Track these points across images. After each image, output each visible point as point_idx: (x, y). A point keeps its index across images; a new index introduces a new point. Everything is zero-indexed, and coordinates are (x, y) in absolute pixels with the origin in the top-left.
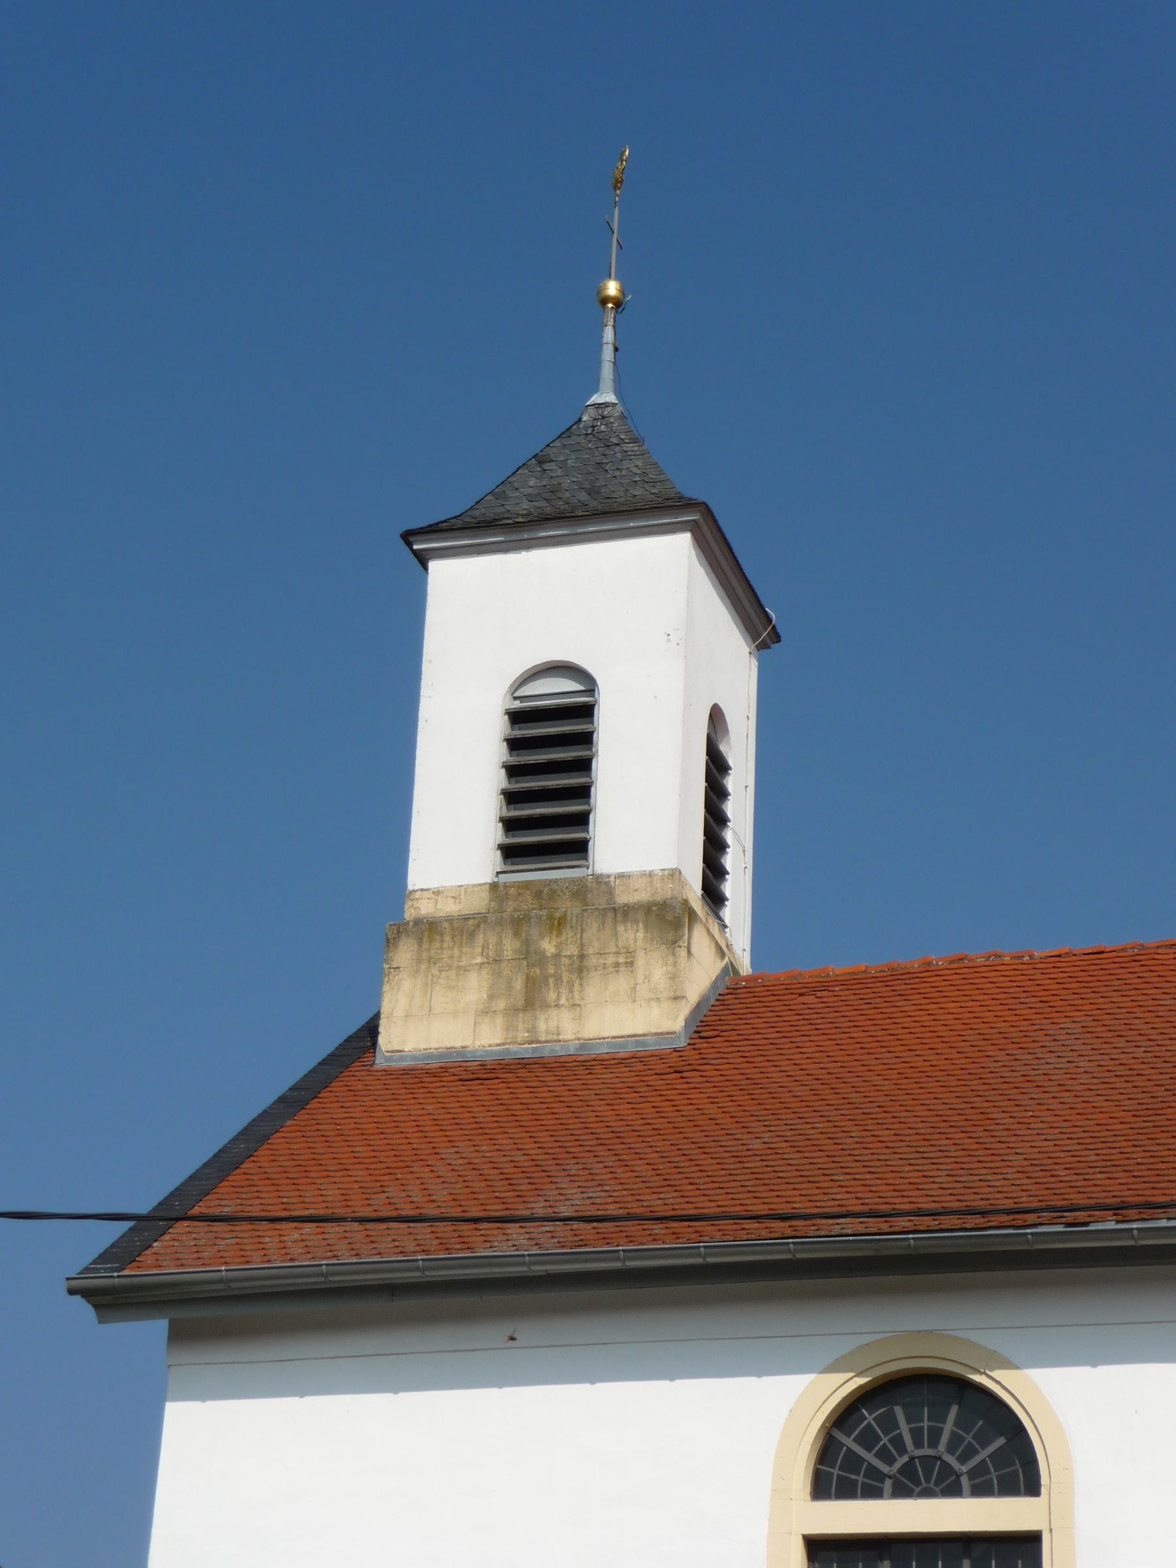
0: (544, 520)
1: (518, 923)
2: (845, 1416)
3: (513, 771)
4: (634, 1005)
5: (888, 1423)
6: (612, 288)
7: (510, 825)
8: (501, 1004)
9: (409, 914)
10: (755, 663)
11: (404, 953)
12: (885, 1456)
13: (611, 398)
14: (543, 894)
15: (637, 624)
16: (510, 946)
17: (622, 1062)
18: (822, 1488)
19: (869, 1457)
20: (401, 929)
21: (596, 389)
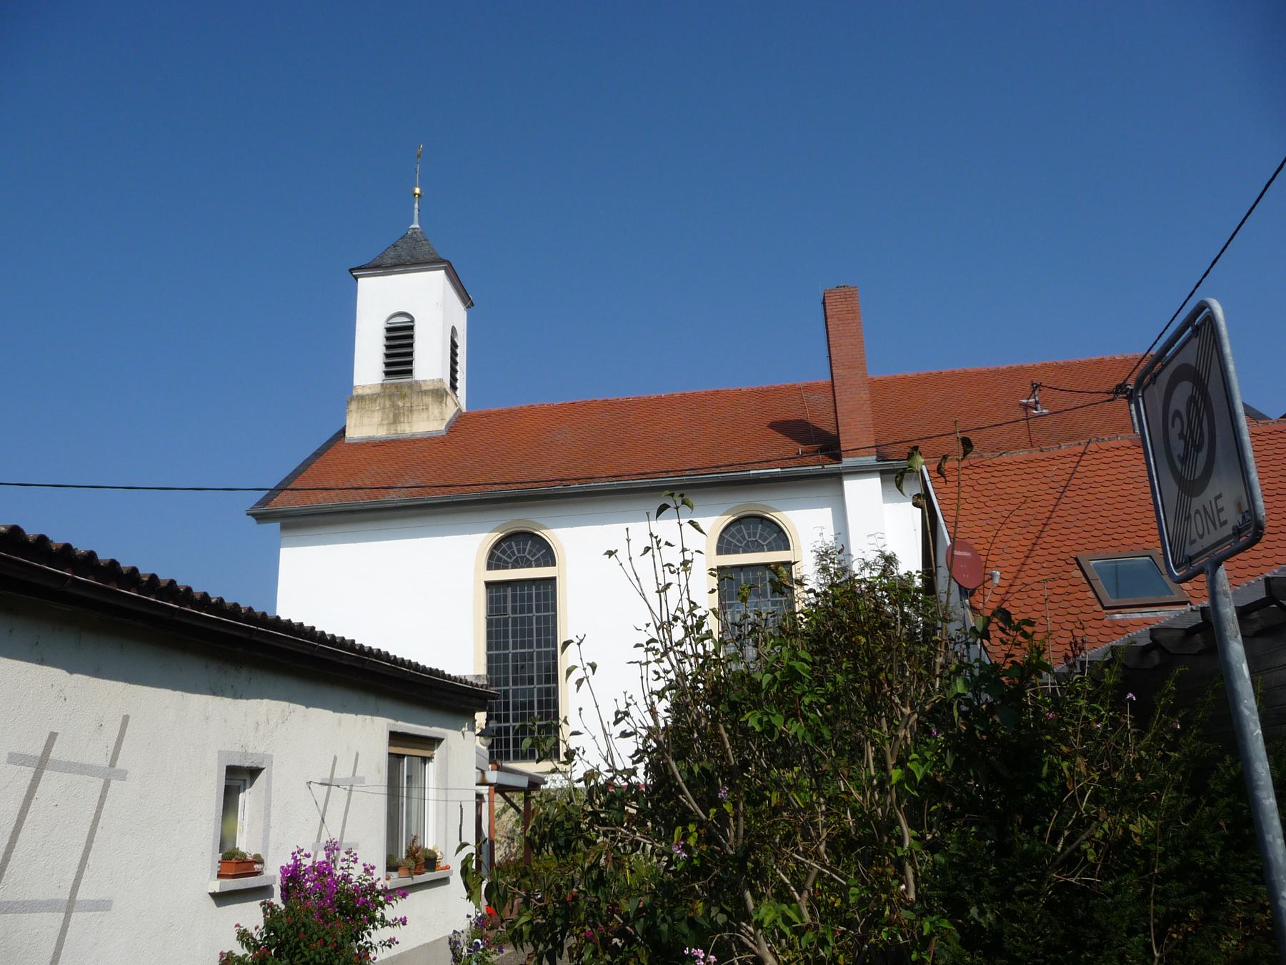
1: (391, 396)
2: (497, 546)
4: (428, 422)
5: (510, 547)
6: (417, 190)
7: (387, 365)
9: (355, 393)
11: (353, 406)
15: (427, 299)
18: (489, 567)
20: (352, 398)
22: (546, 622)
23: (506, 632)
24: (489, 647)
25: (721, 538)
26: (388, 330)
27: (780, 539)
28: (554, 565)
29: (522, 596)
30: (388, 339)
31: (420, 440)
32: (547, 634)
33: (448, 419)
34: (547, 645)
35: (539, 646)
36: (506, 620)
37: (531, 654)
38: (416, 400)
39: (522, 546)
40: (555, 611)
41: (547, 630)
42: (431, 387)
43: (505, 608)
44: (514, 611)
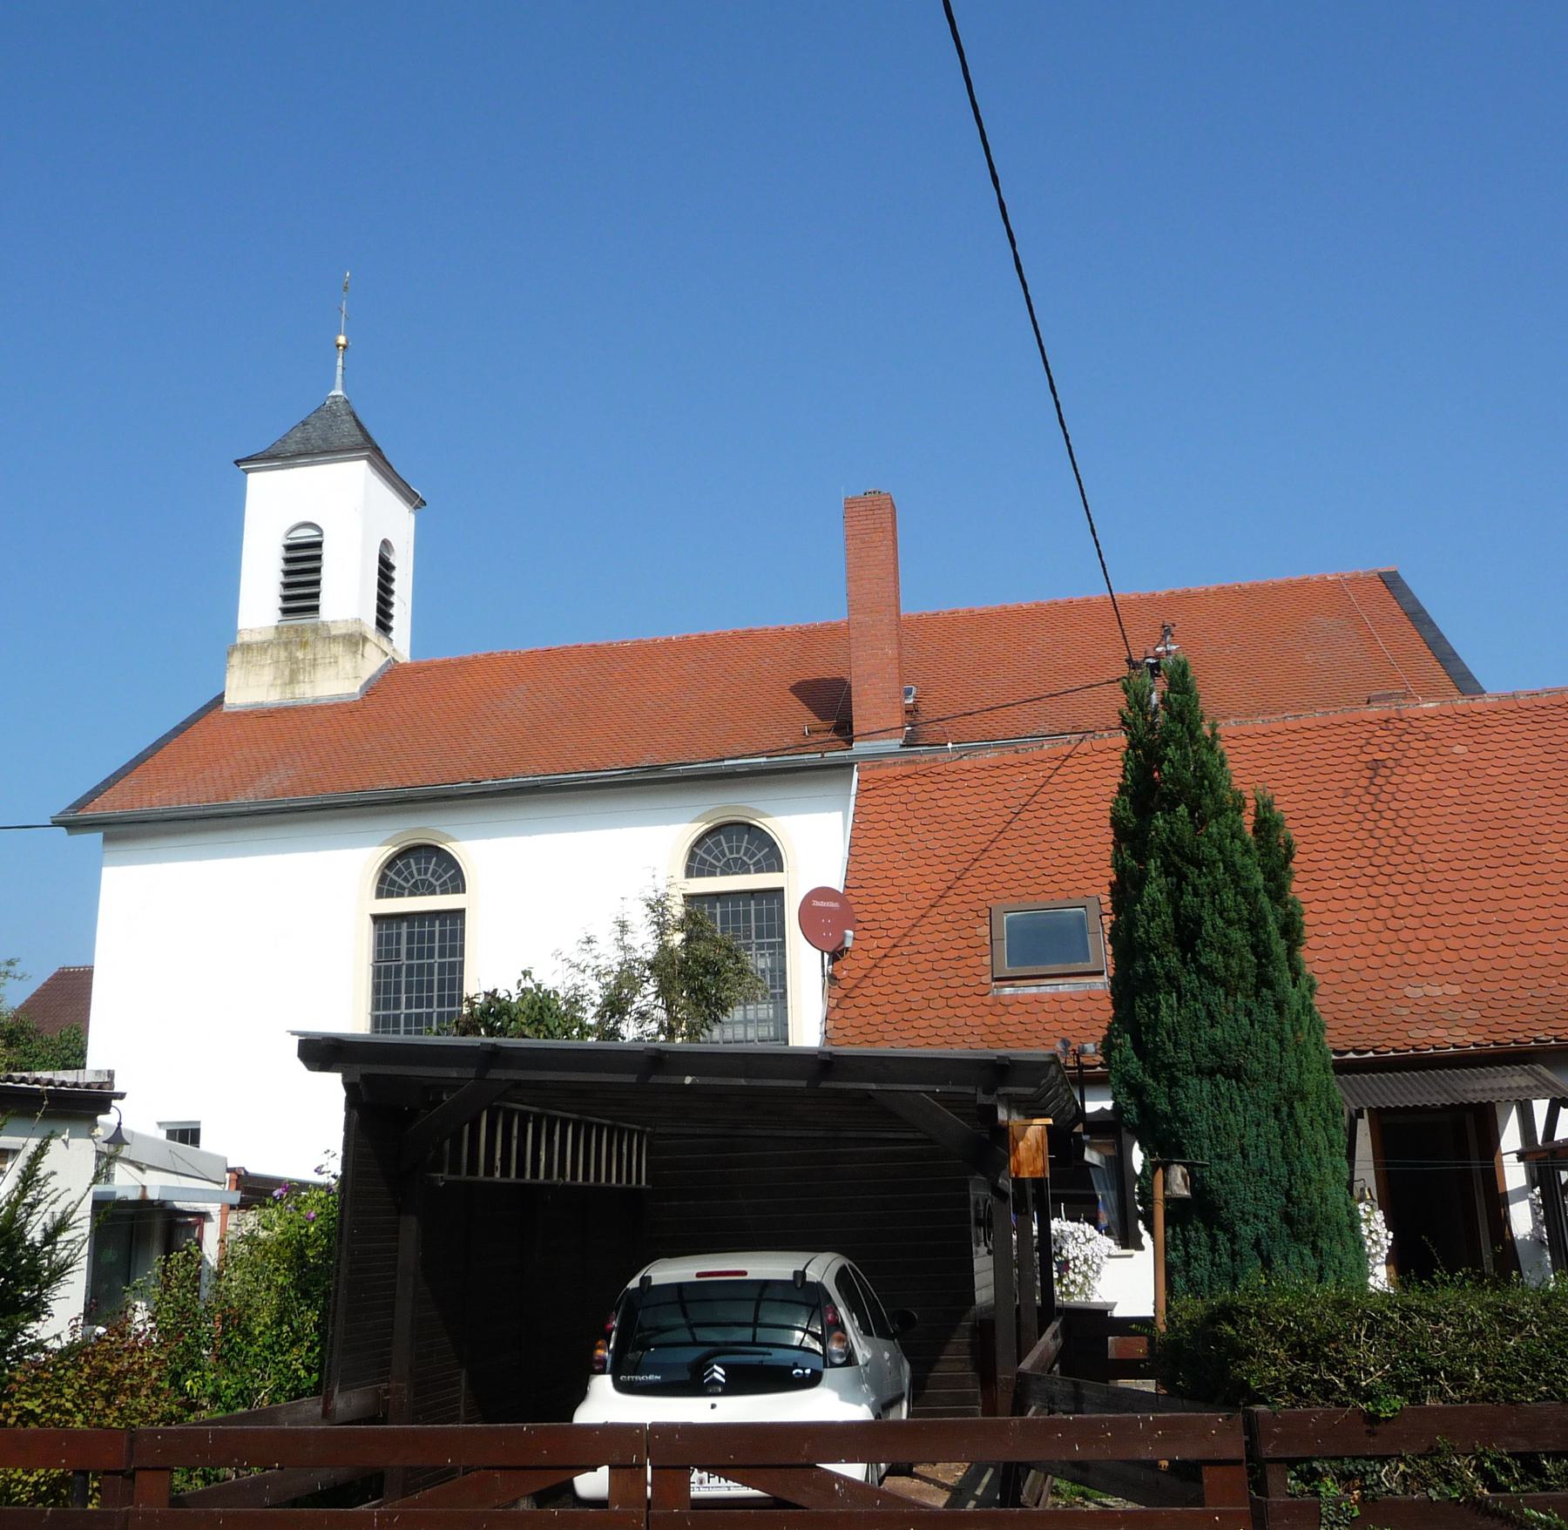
0: (300, 455)
1: (286, 644)
2: (390, 864)
3: (287, 573)
4: (337, 681)
5: (408, 866)
6: (342, 340)
7: (286, 598)
8: (279, 682)
9: (239, 641)
10: (412, 517)
11: (236, 659)
12: (716, 858)
13: (340, 393)
14: (298, 631)
15: (347, 507)
16: (283, 655)
17: (329, 707)
18: (380, 894)
19: (400, 881)
20: (234, 648)
21: (333, 388)
22: (452, 971)
23: (398, 984)
24: (376, 1005)
25: (692, 855)
26: (289, 548)
27: (771, 857)
28: (781, 870)
29: (421, 934)
30: (287, 561)
31: (321, 708)
32: (452, 988)
33: (366, 677)
34: (452, 1004)
35: (441, 1004)
36: (399, 968)
37: (430, 1015)
38: (321, 650)
39: (420, 865)
40: (784, 937)
41: (452, 981)
42: (343, 631)
43: (398, 952)
44: (410, 956)
